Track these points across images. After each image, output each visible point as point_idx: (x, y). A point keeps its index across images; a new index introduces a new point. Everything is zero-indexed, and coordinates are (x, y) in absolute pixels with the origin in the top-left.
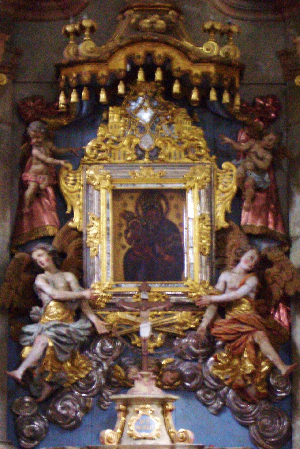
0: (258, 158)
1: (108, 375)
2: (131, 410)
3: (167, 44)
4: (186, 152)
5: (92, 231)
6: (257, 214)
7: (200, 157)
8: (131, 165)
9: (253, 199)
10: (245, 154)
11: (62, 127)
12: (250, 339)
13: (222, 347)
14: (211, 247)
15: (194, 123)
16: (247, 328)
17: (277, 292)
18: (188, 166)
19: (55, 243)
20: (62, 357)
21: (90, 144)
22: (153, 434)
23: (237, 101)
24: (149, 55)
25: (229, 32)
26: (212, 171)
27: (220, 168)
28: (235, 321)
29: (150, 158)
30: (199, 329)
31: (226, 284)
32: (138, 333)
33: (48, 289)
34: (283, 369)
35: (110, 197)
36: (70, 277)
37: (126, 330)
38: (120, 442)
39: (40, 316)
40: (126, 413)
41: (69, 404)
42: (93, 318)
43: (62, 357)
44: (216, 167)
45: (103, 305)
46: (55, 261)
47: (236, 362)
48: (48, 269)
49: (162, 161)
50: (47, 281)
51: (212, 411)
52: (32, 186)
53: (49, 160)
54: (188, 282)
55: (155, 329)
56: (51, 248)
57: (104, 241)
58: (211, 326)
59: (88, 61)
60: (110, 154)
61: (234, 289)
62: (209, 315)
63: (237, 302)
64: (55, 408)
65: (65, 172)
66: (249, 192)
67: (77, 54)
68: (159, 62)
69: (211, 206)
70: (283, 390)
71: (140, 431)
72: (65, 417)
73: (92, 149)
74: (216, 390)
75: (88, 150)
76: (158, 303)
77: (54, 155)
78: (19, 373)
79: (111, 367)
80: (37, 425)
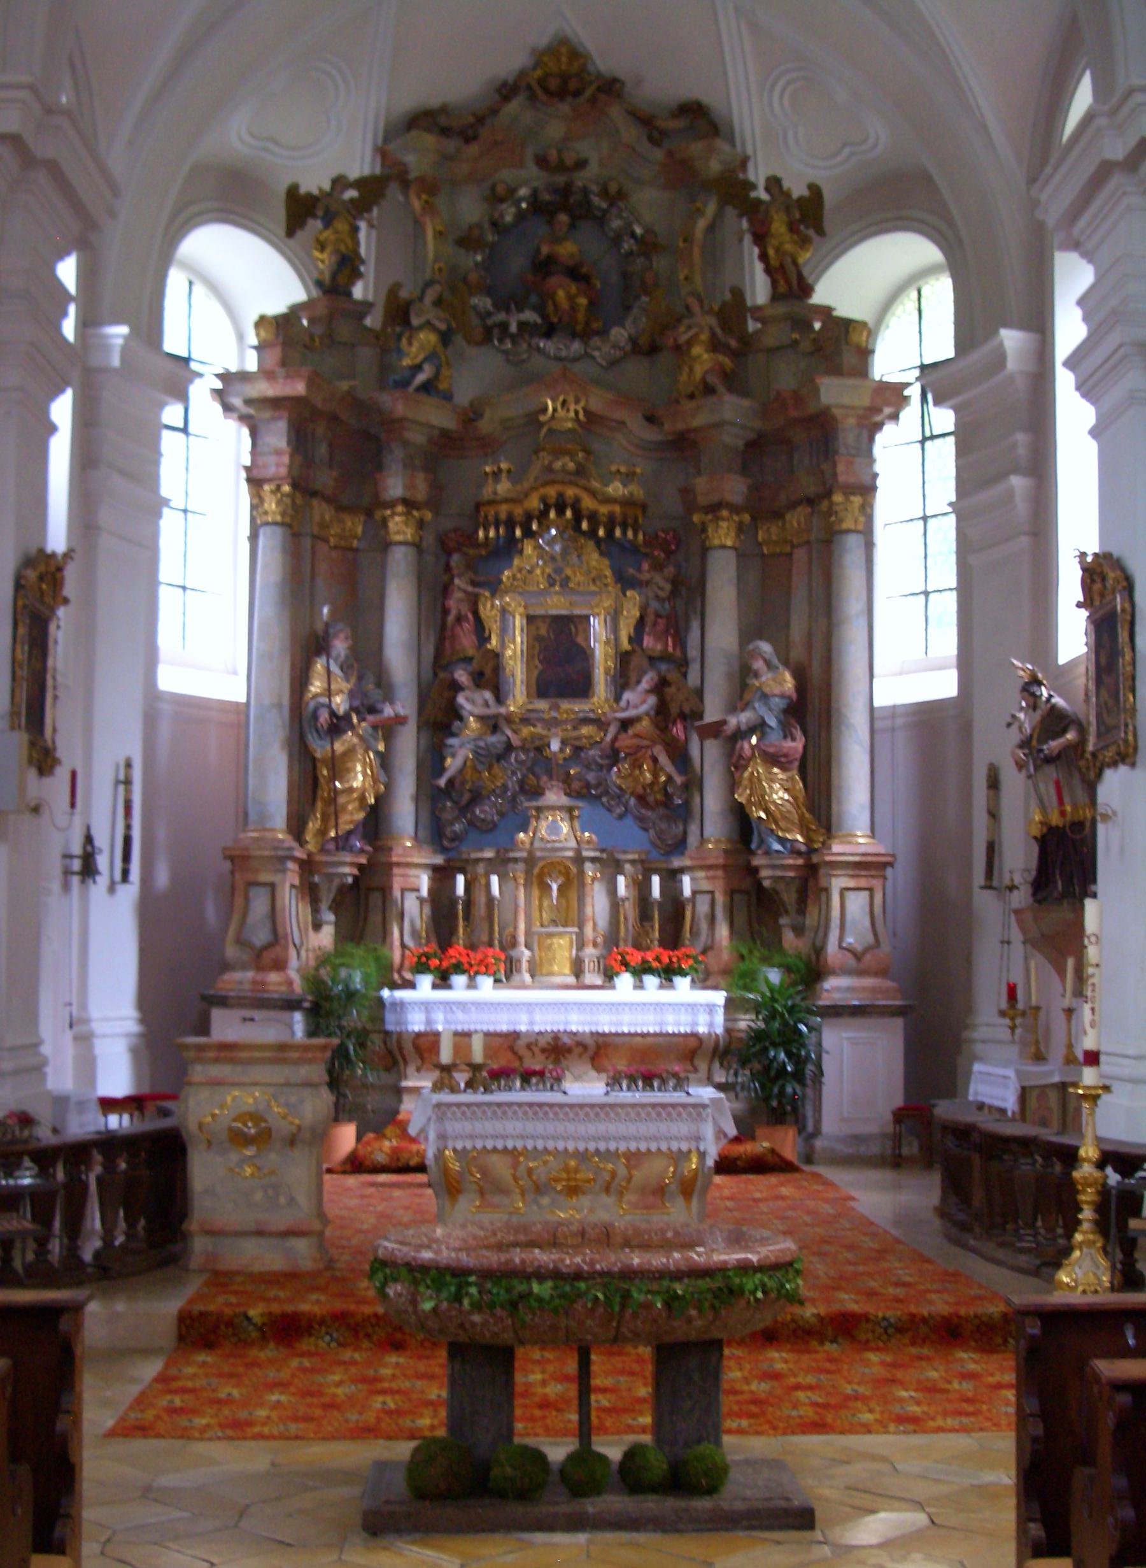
0: (659, 588)
1: (522, 783)
2: (542, 816)
3: (577, 485)
4: (594, 581)
5: (509, 653)
6: (658, 638)
7: (606, 585)
8: (543, 593)
9: (655, 624)
10: (648, 583)
11: (481, 556)
12: (649, 753)
13: (625, 758)
14: (615, 668)
15: (602, 554)
16: (646, 743)
17: (674, 710)
18: (594, 594)
19: (475, 662)
20: (480, 767)
21: (506, 573)
22: (562, 838)
23: (640, 537)
24: (561, 495)
25: (634, 473)
26: (617, 597)
27: (625, 595)
28: (636, 736)
29: (561, 585)
30: (604, 744)
31: (628, 702)
32: (549, 746)
33: (468, 706)
34: (679, 779)
35: (525, 622)
36: (488, 695)
37: (538, 743)
38: (532, 844)
39: (460, 729)
40: (538, 818)
41: (487, 808)
42: (509, 733)
43: (480, 767)
44: (621, 594)
45: (517, 720)
46: (474, 680)
47: (637, 772)
48: (468, 688)
49: (571, 589)
50: (467, 699)
51: (615, 815)
52: (454, 613)
53: (470, 589)
54: (595, 699)
55: (564, 743)
56: (470, 669)
57: (519, 663)
58: (615, 739)
59: (506, 501)
60: (525, 583)
61: (636, 707)
62: (612, 730)
63: (638, 719)
64: (473, 812)
65: (483, 599)
66: (650, 619)
67: (495, 493)
68: (569, 501)
69: (615, 630)
70: (680, 797)
71: (549, 835)
72: (483, 820)
73: (508, 578)
74: (619, 797)
75: (504, 579)
76: (566, 721)
77: (474, 584)
78: (442, 782)
79: (524, 776)
80: (457, 827)
